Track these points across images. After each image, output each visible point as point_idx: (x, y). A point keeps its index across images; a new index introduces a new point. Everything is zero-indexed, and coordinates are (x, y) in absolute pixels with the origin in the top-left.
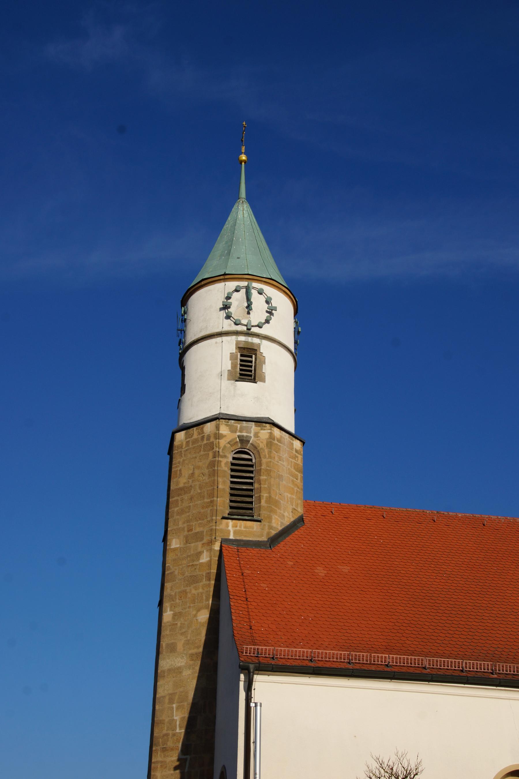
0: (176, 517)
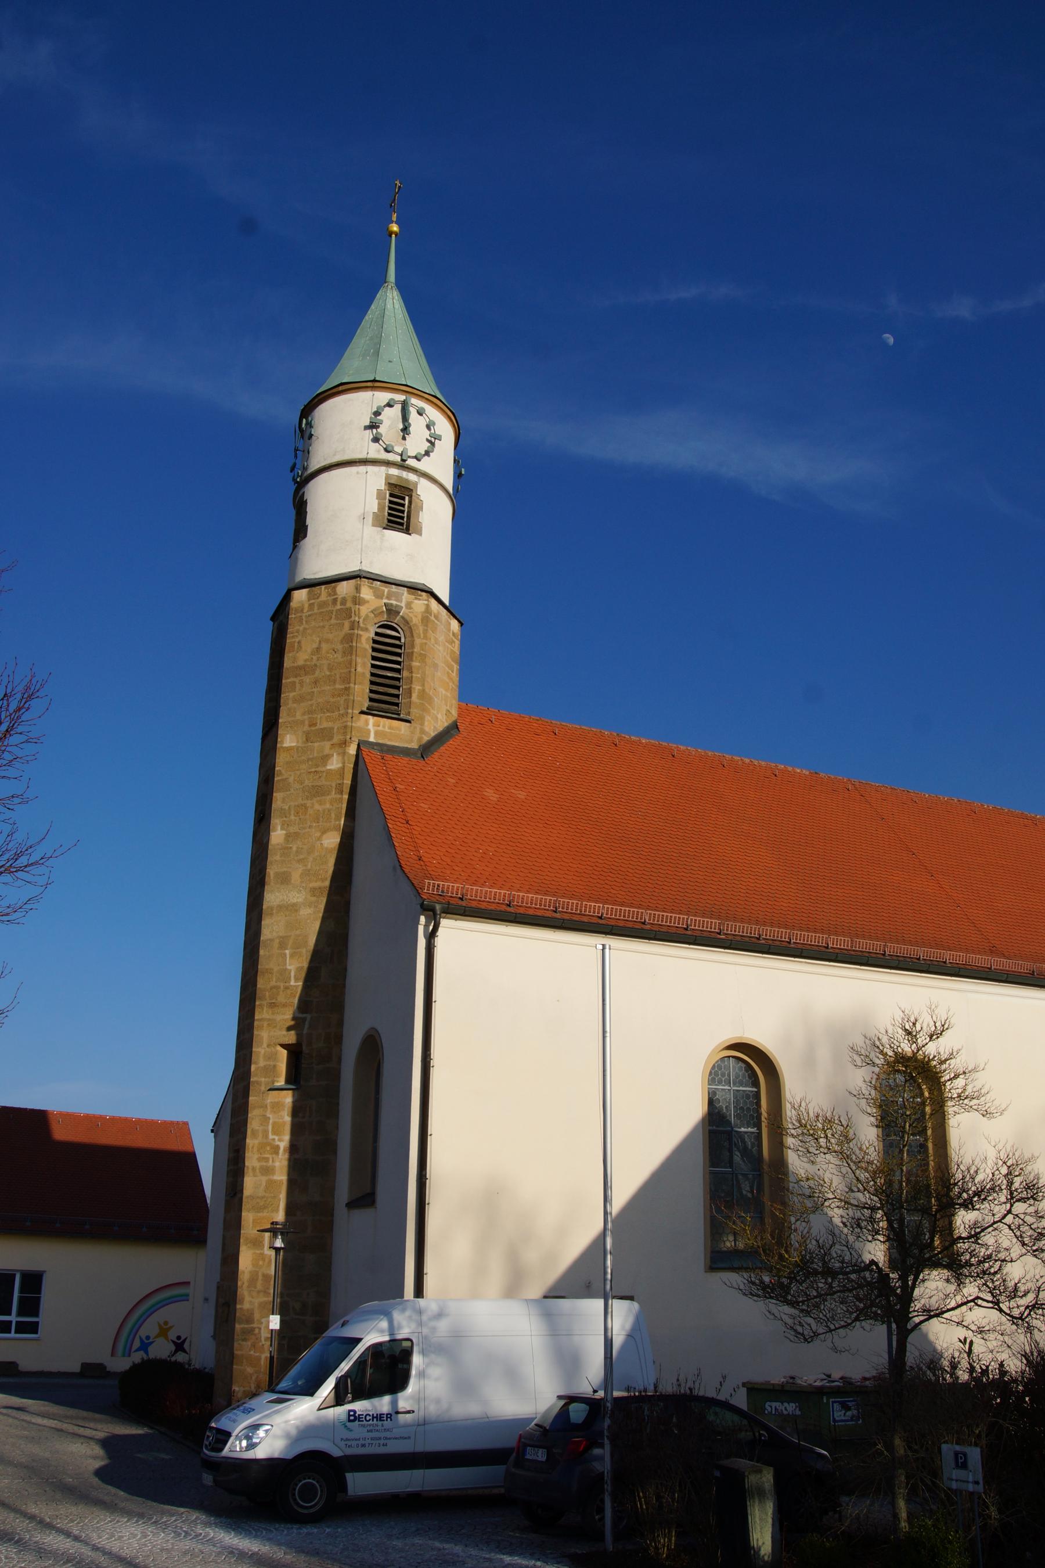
0: (291, 705)
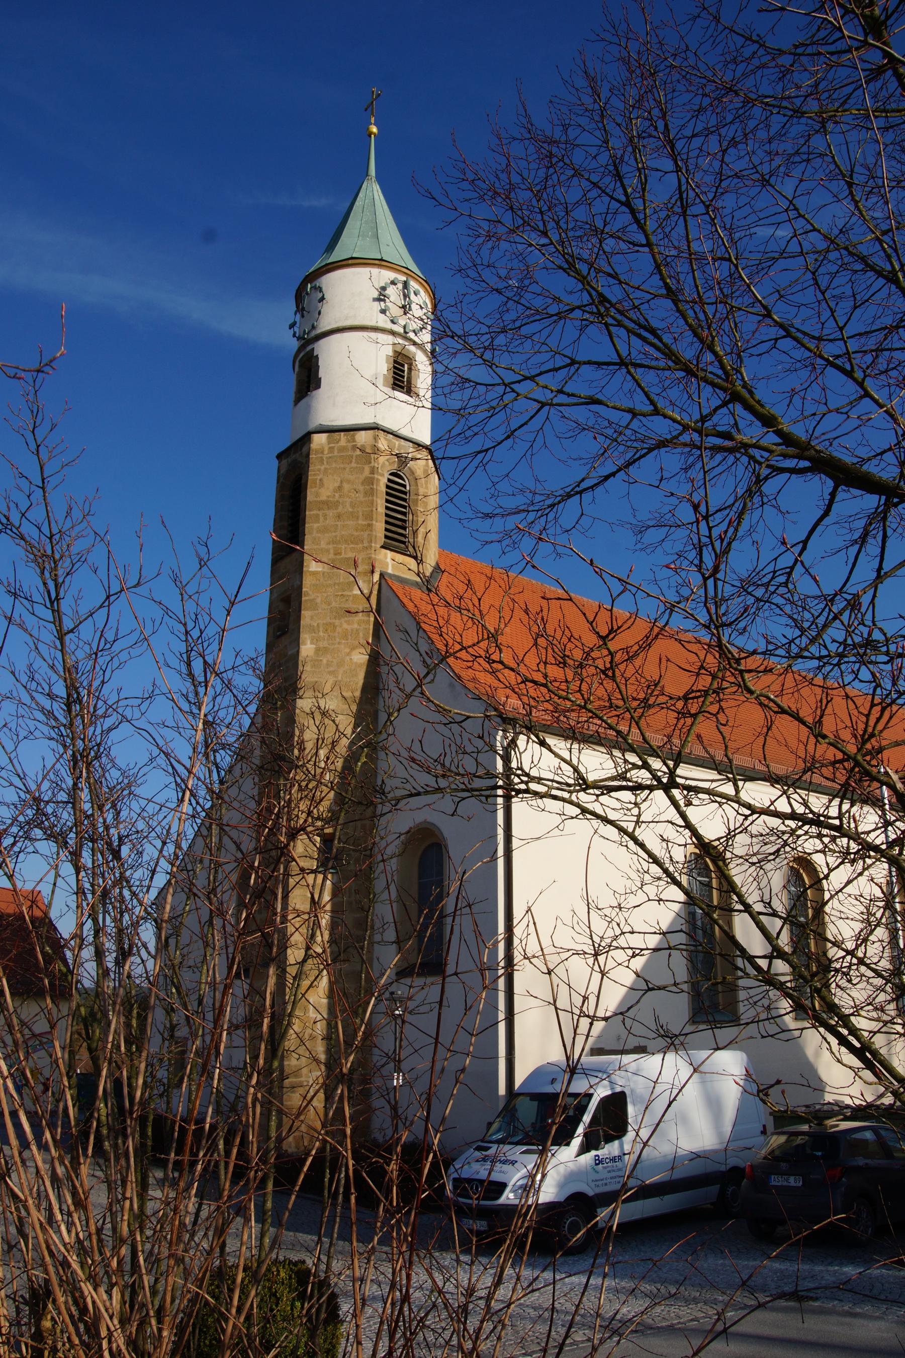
0: (315, 534)
